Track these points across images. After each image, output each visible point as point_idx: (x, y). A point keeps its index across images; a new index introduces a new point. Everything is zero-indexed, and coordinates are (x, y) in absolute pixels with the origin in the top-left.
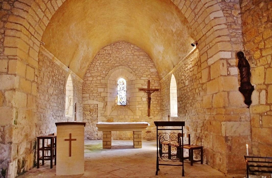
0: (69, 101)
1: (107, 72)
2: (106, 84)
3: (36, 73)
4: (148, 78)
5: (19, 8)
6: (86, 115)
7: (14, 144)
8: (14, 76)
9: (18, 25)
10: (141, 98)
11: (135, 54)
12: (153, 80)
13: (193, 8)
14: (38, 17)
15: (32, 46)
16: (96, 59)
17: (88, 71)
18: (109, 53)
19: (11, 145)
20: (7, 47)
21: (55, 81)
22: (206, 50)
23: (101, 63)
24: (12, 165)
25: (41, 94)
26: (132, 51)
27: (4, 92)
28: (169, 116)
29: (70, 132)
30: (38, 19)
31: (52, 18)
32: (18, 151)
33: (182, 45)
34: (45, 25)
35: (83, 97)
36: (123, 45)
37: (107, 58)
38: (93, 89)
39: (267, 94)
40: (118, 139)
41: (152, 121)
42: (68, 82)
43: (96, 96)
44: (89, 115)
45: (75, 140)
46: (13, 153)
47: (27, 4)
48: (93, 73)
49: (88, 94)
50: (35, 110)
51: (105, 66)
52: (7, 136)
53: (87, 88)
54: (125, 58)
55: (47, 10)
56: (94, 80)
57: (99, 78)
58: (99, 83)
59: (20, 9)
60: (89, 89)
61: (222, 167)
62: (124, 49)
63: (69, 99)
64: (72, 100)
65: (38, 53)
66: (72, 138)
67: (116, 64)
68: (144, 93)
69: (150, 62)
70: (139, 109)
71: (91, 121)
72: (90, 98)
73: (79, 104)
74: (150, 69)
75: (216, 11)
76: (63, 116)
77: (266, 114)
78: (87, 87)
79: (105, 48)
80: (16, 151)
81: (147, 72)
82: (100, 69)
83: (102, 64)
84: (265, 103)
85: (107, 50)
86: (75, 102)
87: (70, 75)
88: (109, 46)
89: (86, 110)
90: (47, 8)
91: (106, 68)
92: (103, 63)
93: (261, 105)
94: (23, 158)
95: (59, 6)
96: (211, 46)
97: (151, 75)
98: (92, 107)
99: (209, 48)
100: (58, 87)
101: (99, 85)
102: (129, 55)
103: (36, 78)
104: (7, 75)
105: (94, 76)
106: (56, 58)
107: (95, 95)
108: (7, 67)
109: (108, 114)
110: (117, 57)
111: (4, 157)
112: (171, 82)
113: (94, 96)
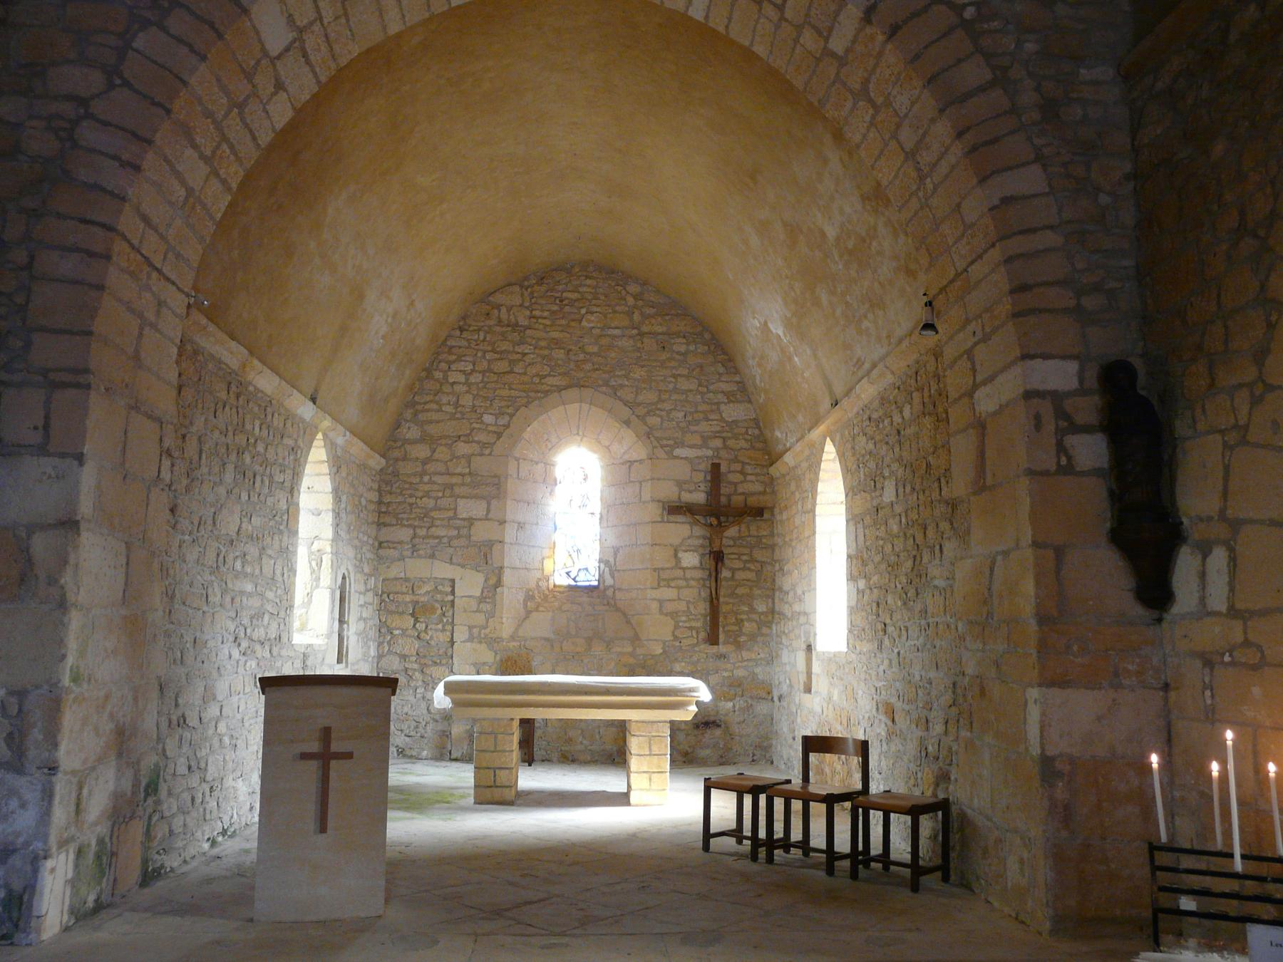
0: (314, 564)
1: (503, 421)
2: (496, 480)
3: (167, 443)
4: (710, 453)
5: (102, 153)
6: (396, 632)
7: (66, 773)
8: (76, 463)
9: (95, 229)
10: (676, 555)
11: (645, 329)
12: (736, 460)
13: (909, 146)
14: (183, 182)
15: (153, 319)
16: (450, 353)
17: (408, 414)
18: (517, 325)
19: (54, 779)
20: (43, 329)
21: (249, 474)
22: (970, 344)
23: (473, 371)
24: (53, 870)
25: (187, 537)
26: (630, 314)
27: (29, 537)
28: (809, 648)
29: (327, 723)
30: (183, 193)
31: (248, 178)
32: (78, 805)
33: (867, 306)
34: (212, 218)
35: (380, 543)
36: (589, 282)
37: (505, 346)
38: (431, 503)
39: (1235, 565)
40: (555, 756)
41: (726, 670)
42: (309, 469)
43: (445, 540)
44: (409, 632)
45: (349, 756)
46: (60, 814)
47: (134, 135)
48: (431, 422)
49: (408, 526)
50: (160, 613)
51: (495, 390)
52: (36, 734)
53: (400, 499)
54: (595, 349)
55: (225, 146)
56: (436, 456)
57: (463, 449)
58: (463, 475)
59: (106, 155)
60: (411, 505)
61: (1030, 903)
62: (590, 301)
63: (312, 553)
64: (327, 559)
65: (179, 348)
66: (335, 747)
67: (550, 380)
68: (688, 527)
69: (722, 370)
70: (661, 607)
71: (416, 666)
72: (414, 546)
73: (359, 576)
74: (723, 407)
75: (1010, 168)
76: (284, 639)
77: (1227, 658)
78: (401, 494)
79: (498, 298)
80: (73, 808)
81: (707, 419)
82: (467, 401)
83: (480, 377)
84: (1224, 609)
85: (504, 310)
86: (343, 570)
87: (320, 436)
88: (517, 288)
89: (393, 608)
90: (225, 139)
91: (502, 399)
92: (483, 372)
93: (1209, 614)
94: (101, 842)
95: (279, 126)
96: (988, 330)
97: (724, 439)
98: (428, 592)
99: (979, 335)
100: (262, 498)
101: (463, 484)
102: (617, 332)
103: (166, 463)
104: (44, 460)
105: (441, 438)
106: (256, 362)
107: (442, 532)
108: (40, 424)
109: (506, 630)
110: (557, 343)
111: (18, 834)
112: (822, 475)
113: (437, 537)
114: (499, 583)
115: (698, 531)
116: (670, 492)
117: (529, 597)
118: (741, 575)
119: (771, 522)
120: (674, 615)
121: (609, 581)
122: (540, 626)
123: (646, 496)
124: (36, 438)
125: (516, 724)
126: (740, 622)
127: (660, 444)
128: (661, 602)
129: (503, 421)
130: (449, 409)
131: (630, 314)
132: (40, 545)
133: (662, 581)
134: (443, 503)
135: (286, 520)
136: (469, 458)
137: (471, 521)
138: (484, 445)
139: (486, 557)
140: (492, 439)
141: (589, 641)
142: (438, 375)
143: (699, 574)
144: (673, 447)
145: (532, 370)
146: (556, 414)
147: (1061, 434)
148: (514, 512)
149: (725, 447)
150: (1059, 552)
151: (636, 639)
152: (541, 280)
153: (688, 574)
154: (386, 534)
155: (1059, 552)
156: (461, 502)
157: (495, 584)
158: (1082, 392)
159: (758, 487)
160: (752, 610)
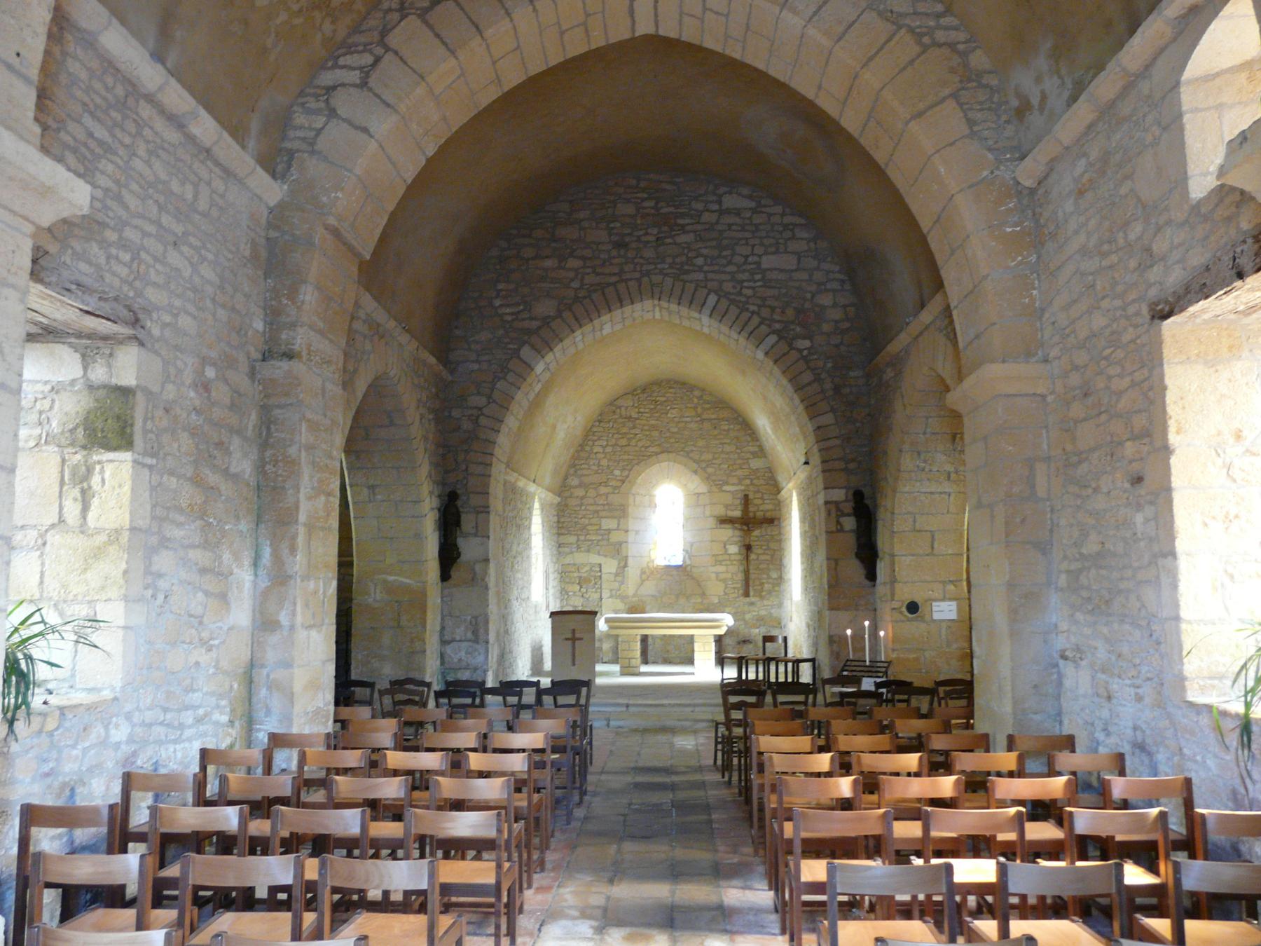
1: (626, 473)
11: (705, 416)
12: (758, 491)
17: (572, 471)
26: (695, 408)
52: (482, 631)
57: (603, 490)
66: (577, 635)
67: (651, 449)
79: (619, 402)
82: (604, 462)
109: (631, 591)
110: (654, 427)
114: (626, 566)
115: (737, 533)
116: (720, 511)
117: (643, 572)
118: (762, 557)
119: (779, 526)
120: (724, 581)
121: (688, 562)
122: (650, 588)
123: (708, 513)
124: (473, 531)
125: (639, 638)
126: (762, 584)
127: (715, 483)
128: (717, 574)
129: (626, 473)
130: (595, 468)
131: (695, 408)
132: (478, 567)
133: (718, 562)
134: (594, 521)
135: (527, 542)
136: (607, 495)
137: (609, 531)
138: (616, 488)
139: (618, 551)
140: (619, 484)
141: (677, 597)
142: (588, 448)
143: (739, 557)
144: (722, 485)
145: (640, 444)
146: (655, 468)
147: (838, 517)
148: (632, 524)
149: (752, 484)
150: (836, 561)
151: (703, 595)
152: (644, 390)
153: (733, 557)
154: (564, 539)
155: (836, 561)
156: (604, 521)
157: (624, 565)
158: (846, 501)
159: (770, 507)
160: (769, 577)
